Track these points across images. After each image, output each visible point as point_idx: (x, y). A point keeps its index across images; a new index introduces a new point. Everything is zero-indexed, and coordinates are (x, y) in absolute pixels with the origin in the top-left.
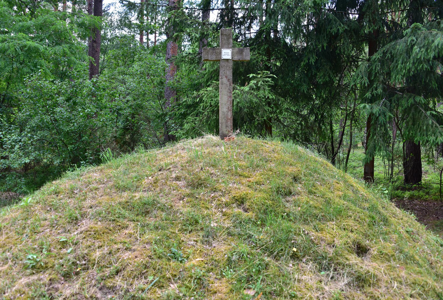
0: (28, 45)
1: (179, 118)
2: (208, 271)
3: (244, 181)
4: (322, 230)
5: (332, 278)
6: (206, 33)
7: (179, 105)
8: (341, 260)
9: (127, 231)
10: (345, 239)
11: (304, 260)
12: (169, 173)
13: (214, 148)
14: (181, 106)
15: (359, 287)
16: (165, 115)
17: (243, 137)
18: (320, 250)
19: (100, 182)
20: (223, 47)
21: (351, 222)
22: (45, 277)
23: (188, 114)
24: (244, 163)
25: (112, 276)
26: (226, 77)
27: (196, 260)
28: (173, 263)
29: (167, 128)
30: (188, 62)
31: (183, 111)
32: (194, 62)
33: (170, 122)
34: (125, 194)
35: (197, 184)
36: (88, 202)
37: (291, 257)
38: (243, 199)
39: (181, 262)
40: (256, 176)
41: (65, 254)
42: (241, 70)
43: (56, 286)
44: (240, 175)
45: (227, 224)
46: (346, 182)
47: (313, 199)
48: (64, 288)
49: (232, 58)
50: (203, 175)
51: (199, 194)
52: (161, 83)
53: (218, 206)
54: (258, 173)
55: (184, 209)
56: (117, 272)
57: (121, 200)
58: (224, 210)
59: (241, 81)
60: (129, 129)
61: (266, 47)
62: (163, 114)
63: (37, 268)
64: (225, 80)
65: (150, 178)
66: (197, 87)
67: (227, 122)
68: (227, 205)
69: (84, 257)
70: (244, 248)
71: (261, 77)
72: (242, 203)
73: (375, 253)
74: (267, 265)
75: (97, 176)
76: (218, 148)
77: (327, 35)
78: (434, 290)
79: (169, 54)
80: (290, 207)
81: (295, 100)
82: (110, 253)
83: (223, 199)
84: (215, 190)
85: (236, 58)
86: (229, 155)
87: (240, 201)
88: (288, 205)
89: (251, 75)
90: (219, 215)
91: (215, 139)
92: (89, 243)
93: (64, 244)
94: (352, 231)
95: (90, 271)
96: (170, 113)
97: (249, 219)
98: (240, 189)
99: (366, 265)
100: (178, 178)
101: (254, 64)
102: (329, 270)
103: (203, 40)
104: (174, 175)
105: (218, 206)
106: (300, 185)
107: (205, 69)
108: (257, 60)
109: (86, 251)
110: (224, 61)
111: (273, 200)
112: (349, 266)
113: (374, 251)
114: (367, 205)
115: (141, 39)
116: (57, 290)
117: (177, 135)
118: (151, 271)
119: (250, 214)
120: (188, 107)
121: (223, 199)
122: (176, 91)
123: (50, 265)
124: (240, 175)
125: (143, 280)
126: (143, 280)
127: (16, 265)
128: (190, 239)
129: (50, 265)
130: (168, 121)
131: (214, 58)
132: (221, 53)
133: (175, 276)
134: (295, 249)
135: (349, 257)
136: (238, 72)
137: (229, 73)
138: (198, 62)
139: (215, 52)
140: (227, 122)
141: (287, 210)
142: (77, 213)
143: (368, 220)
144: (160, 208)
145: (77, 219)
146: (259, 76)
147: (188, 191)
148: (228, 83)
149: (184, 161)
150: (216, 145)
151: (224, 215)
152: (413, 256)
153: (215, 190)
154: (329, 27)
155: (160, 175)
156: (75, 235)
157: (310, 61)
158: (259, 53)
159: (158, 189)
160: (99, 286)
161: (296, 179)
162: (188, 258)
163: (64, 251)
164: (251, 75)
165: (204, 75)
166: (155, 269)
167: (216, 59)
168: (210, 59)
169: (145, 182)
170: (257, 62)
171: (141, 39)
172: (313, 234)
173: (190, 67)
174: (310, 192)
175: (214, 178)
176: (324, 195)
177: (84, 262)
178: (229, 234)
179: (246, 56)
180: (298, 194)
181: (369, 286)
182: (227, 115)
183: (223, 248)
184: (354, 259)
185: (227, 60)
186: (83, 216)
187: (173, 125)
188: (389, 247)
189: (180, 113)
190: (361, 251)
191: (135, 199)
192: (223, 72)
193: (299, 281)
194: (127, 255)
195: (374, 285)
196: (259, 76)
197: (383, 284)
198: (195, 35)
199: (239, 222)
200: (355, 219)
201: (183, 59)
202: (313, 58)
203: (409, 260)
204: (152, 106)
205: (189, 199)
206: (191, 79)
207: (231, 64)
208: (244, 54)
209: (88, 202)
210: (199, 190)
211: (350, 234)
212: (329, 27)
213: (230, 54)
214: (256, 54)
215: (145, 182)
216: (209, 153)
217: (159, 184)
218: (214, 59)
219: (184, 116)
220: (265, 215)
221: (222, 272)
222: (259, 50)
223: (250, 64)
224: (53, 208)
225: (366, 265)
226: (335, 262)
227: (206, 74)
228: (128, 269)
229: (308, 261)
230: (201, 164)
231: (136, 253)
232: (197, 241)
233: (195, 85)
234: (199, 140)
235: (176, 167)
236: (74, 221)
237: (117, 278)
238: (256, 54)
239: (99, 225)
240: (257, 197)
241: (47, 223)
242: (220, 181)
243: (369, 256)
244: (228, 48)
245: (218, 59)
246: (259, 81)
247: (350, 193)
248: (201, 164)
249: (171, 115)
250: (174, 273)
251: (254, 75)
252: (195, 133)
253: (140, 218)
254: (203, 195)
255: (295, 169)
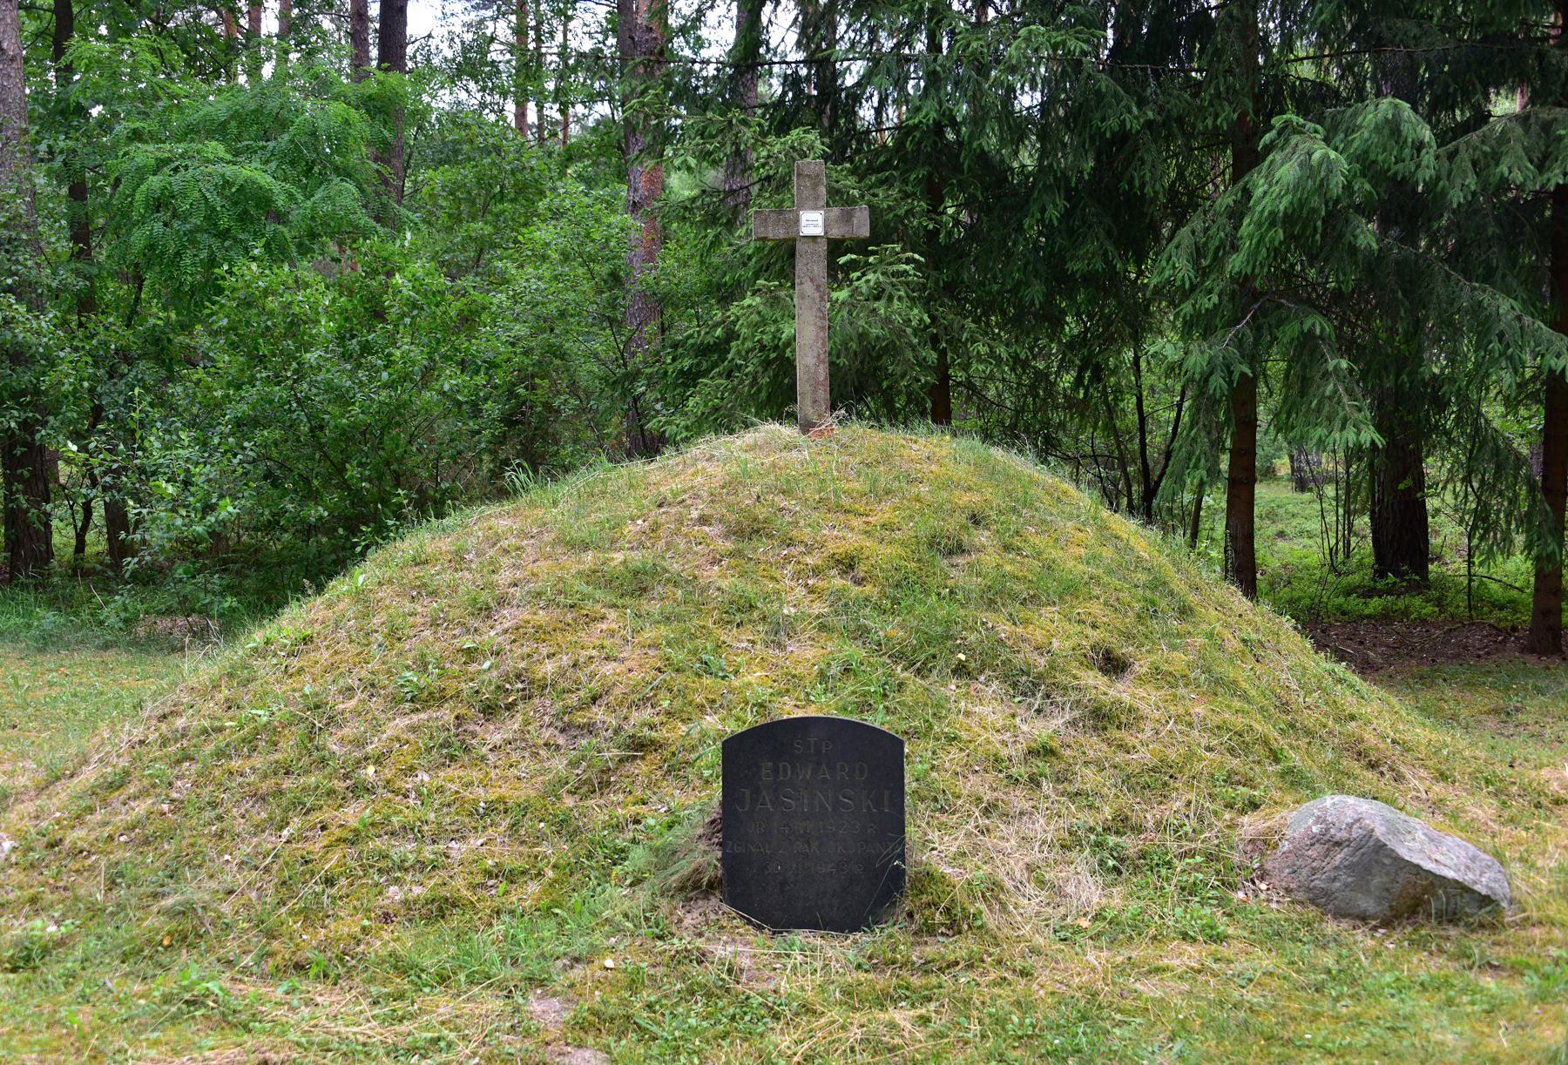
0: (240, 181)
1: (676, 387)
2: (780, 694)
3: (857, 522)
4: (1027, 622)
5: (1039, 711)
7: (675, 346)
8: (1061, 678)
9: (604, 626)
10: (1074, 641)
11: (982, 678)
12: (685, 511)
13: (784, 454)
14: (680, 350)
15: (1095, 729)
16: (633, 376)
17: (856, 427)
18: (1018, 660)
19: (523, 534)
20: (802, 207)
21: (1096, 608)
22: (447, 714)
23: (705, 374)
24: (857, 486)
25: (582, 707)
27: (755, 676)
28: (707, 681)
29: (638, 412)
31: (686, 363)
33: (651, 396)
34: (589, 557)
35: (748, 530)
36: (504, 577)
37: (954, 672)
38: (852, 558)
39: (723, 678)
40: (884, 512)
41: (479, 672)
43: (471, 728)
44: (847, 511)
45: (819, 608)
46: (1103, 528)
47: (1012, 562)
48: (487, 732)
50: (762, 512)
51: (755, 550)
52: (615, 279)
53: (797, 576)
54: (886, 506)
55: (723, 580)
56: (594, 700)
57: (581, 567)
58: (810, 582)
60: (517, 422)
61: (922, 173)
62: (626, 376)
63: (423, 699)
64: (808, 288)
65: (640, 522)
66: (727, 294)
67: (815, 391)
68: (816, 571)
69: (518, 676)
70: (854, 651)
72: (851, 567)
73: (1145, 669)
74: (900, 685)
75: (503, 524)
76: (794, 453)
77: (1092, 139)
78: (1266, 742)
79: (636, 190)
80: (958, 577)
81: (1018, 323)
82: (574, 665)
83: (809, 560)
84: (790, 542)
85: (836, 233)
86: (821, 469)
87: (847, 564)
88: (953, 573)
90: (800, 592)
91: (787, 432)
92: (526, 650)
93: (471, 654)
94: (1094, 626)
95: (536, 701)
96: (648, 371)
97: (866, 599)
98: (849, 540)
99: (1121, 692)
100: (703, 520)
102: (1034, 695)
104: (695, 514)
105: (797, 576)
106: (987, 533)
109: (522, 665)
111: (919, 560)
112: (1078, 689)
113: (1141, 667)
114: (1142, 577)
115: (521, 115)
116: (474, 735)
117: (670, 430)
118: (662, 694)
119: (868, 589)
120: (703, 350)
121: (809, 560)
122: (661, 303)
123: (449, 693)
124: (847, 511)
125: (649, 710)
126: (649, 710)
128: (737, 639)
129: (449, 693)
130: (643, 394)
132: (797, 221)
133: (714, 701)
134: (963, 657)
135: (1079, 674)
138: (729, 221)
140: (815, 391)
141: (949, 583)
142: (485, 597)
143: (1137, 606)
144: (669, 580)
145: (488, 608)
147: (730, 545)
148: (817, 295)
149: (716, 483)
150: (788, 447)
151: (812, 592)
152: (1234, 682)
153: (790, 542)
154: (1098, 115)
155: (666, 516)
156: (491, 636)
157: (1047, 215)
159: (662, 543)
160: (559, 724)
161: (976, 520)
162: (736, 672)
163: (473, 667)
166: (670, 691)
169: (630, 529)
171: (521, 115)
172: (1005, 629)
174: (1007, 548)
175: (788, 518)
176: (1039, 554)
177: (520, 686)
178: (823, 628)
179: (859, 227)
180: (981, 549)
181: (1118, 728)
182: (816, 372)
183: (809, 654)
184: (1093, 679)
185: (814, 238)
186: (502, 601)
187: (658, 407)
188: (1179, 661)
189: (693, 367)
190: (1113, 665)
191: (612, 564)
193: (968, 714)
194: (608, 669)
195: (1128, 726)
197: (1148, 727)
199: (840, 603)
200: (1106, 604)
202: (1056, 205)
203: (1219, 685)
204: (590, 352)
205: (733, 562)
207: (823, 247)
209: (504, 577)
210: (754, 543)
211: (1089, 632)
212: (1098, 115)
213: (821, 222)
215: (630, 529)
216: (774, 465)
217: (661, 532)
219: (689, 378)
220: (902, 588)
221: (808, 694)
222: (905, 182)
224: (423, 590)
225: (1121, 692)
226: (1048, 681)
228: (617, 691)
229: (989, 679)
230: (758, 488)
231: (628, 664)
232: (753, 642)
233: (719, 286)
234: (749, 437)
235: (697, 496)
236: (485, 612)
237: (595, 709)
239: (542, 617)
240: (882, 554)
241: (419, 620)
242: (802, 523)
243: (1128, 676)
244: (815, 208)
247: (1108, 553)
248: (758, 488)
249: (650, 377)
250: (711, 697)
252: (722, 421)
253: (627, 600)
254: (764, 553)
255: (976, 498)
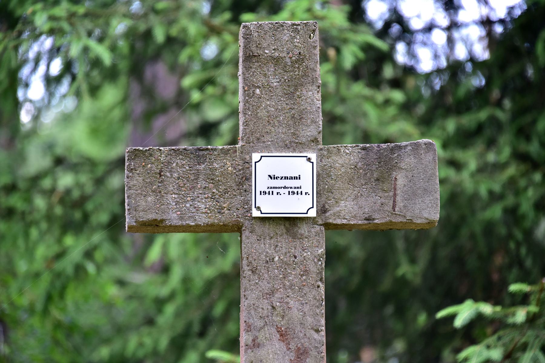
6: (159, 35)
20: (258, 142)
26: (283, 335)
30: (49, 217)
32: (86, 217)
42: (405, 269)
49: (322, 210)
59: (411, 346)
71: (531, 320)
85: (349, 209)
89: (464, 313)
101: (489, 228)
103: (148, 72)
107: (165, 269)
108: (510, 200)
110: (268, 229)
127: (158, 171)
131: (202, 212)
132: (244, 178)
136: (386, 284)
137: (308, 313)
139: (211, 178)
146: (520, 315)
158: (521, 157)
164: (464, 313)
165: (160, 303)
167: (216, 219)
168: (173, 218)
170: (513, 214)
173: (60, 255)
185: (290, 223)
192: (265, 304)
196: (520, 315)
198: (86, 50)
201: (16, 201)
206: (70, 329)
207: (313, 248)
208: (401, 181)
213: (307, 183)
214: (498, 167)
218: (202, 220)
222: (524, 133)
223: (464, 232)
227: (172, 296)
238: (498, 167)
244: (293, 145)
245: (227, 217)
246: (524, 348)
251: (487, 309)
